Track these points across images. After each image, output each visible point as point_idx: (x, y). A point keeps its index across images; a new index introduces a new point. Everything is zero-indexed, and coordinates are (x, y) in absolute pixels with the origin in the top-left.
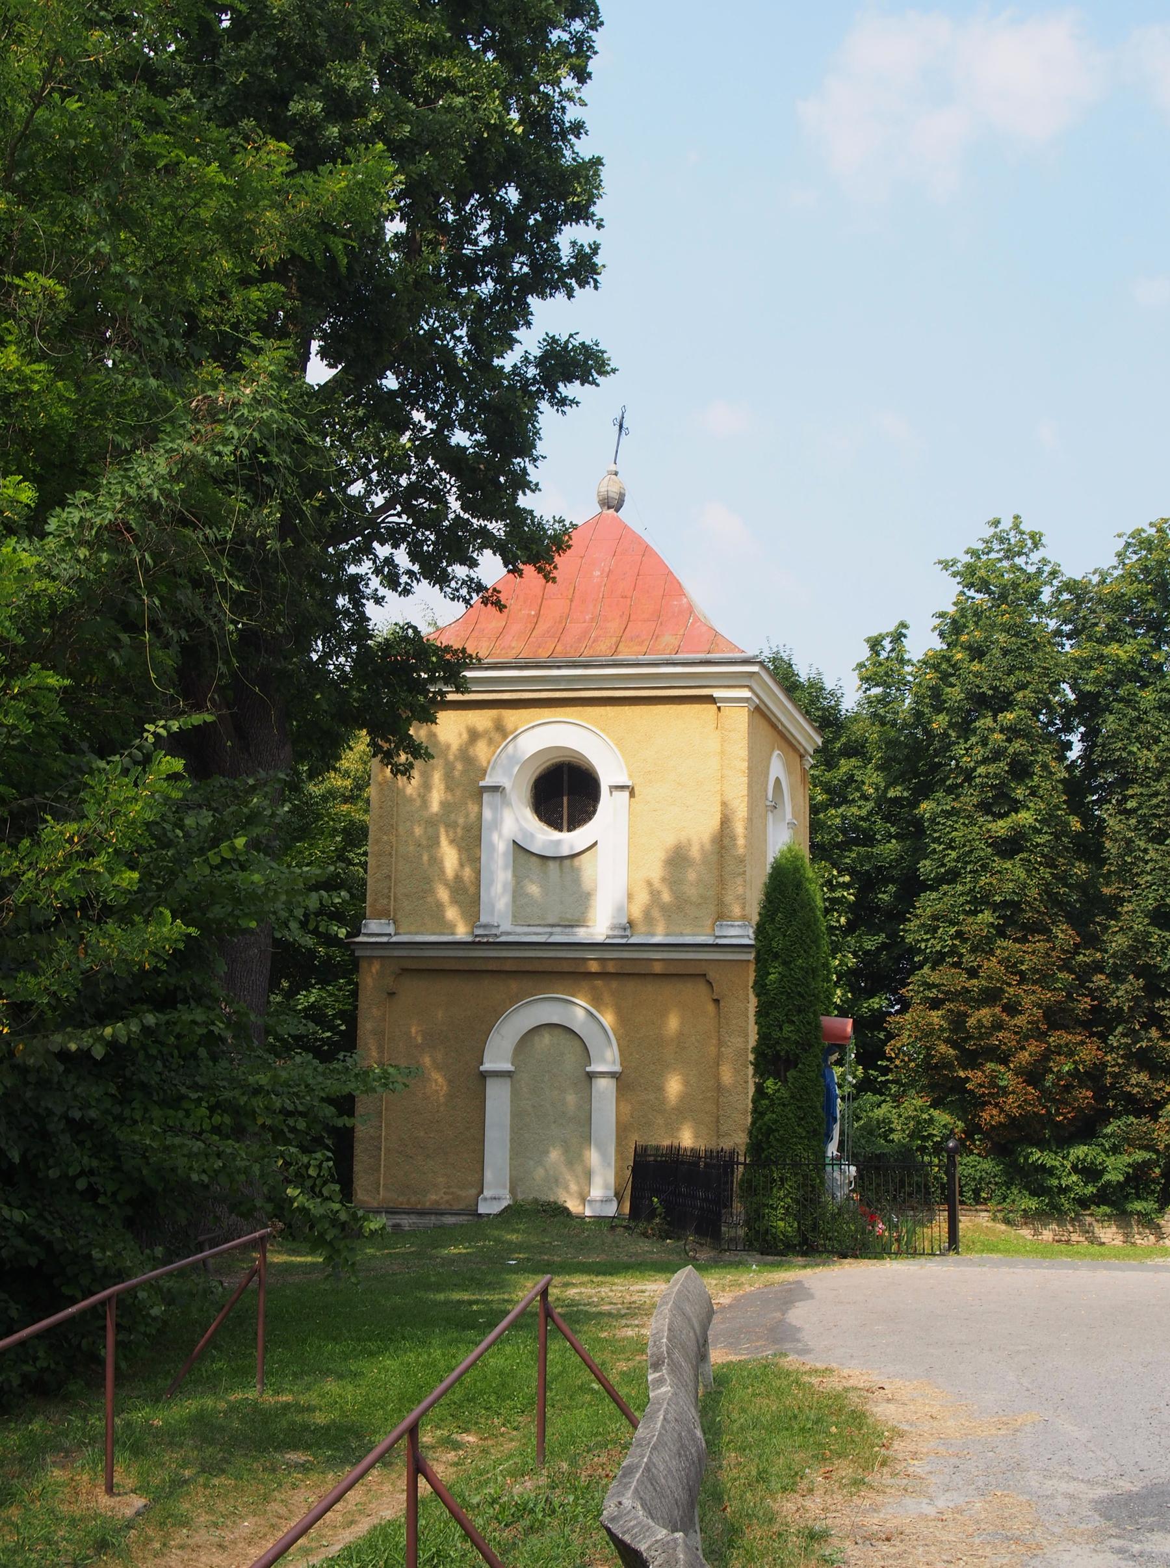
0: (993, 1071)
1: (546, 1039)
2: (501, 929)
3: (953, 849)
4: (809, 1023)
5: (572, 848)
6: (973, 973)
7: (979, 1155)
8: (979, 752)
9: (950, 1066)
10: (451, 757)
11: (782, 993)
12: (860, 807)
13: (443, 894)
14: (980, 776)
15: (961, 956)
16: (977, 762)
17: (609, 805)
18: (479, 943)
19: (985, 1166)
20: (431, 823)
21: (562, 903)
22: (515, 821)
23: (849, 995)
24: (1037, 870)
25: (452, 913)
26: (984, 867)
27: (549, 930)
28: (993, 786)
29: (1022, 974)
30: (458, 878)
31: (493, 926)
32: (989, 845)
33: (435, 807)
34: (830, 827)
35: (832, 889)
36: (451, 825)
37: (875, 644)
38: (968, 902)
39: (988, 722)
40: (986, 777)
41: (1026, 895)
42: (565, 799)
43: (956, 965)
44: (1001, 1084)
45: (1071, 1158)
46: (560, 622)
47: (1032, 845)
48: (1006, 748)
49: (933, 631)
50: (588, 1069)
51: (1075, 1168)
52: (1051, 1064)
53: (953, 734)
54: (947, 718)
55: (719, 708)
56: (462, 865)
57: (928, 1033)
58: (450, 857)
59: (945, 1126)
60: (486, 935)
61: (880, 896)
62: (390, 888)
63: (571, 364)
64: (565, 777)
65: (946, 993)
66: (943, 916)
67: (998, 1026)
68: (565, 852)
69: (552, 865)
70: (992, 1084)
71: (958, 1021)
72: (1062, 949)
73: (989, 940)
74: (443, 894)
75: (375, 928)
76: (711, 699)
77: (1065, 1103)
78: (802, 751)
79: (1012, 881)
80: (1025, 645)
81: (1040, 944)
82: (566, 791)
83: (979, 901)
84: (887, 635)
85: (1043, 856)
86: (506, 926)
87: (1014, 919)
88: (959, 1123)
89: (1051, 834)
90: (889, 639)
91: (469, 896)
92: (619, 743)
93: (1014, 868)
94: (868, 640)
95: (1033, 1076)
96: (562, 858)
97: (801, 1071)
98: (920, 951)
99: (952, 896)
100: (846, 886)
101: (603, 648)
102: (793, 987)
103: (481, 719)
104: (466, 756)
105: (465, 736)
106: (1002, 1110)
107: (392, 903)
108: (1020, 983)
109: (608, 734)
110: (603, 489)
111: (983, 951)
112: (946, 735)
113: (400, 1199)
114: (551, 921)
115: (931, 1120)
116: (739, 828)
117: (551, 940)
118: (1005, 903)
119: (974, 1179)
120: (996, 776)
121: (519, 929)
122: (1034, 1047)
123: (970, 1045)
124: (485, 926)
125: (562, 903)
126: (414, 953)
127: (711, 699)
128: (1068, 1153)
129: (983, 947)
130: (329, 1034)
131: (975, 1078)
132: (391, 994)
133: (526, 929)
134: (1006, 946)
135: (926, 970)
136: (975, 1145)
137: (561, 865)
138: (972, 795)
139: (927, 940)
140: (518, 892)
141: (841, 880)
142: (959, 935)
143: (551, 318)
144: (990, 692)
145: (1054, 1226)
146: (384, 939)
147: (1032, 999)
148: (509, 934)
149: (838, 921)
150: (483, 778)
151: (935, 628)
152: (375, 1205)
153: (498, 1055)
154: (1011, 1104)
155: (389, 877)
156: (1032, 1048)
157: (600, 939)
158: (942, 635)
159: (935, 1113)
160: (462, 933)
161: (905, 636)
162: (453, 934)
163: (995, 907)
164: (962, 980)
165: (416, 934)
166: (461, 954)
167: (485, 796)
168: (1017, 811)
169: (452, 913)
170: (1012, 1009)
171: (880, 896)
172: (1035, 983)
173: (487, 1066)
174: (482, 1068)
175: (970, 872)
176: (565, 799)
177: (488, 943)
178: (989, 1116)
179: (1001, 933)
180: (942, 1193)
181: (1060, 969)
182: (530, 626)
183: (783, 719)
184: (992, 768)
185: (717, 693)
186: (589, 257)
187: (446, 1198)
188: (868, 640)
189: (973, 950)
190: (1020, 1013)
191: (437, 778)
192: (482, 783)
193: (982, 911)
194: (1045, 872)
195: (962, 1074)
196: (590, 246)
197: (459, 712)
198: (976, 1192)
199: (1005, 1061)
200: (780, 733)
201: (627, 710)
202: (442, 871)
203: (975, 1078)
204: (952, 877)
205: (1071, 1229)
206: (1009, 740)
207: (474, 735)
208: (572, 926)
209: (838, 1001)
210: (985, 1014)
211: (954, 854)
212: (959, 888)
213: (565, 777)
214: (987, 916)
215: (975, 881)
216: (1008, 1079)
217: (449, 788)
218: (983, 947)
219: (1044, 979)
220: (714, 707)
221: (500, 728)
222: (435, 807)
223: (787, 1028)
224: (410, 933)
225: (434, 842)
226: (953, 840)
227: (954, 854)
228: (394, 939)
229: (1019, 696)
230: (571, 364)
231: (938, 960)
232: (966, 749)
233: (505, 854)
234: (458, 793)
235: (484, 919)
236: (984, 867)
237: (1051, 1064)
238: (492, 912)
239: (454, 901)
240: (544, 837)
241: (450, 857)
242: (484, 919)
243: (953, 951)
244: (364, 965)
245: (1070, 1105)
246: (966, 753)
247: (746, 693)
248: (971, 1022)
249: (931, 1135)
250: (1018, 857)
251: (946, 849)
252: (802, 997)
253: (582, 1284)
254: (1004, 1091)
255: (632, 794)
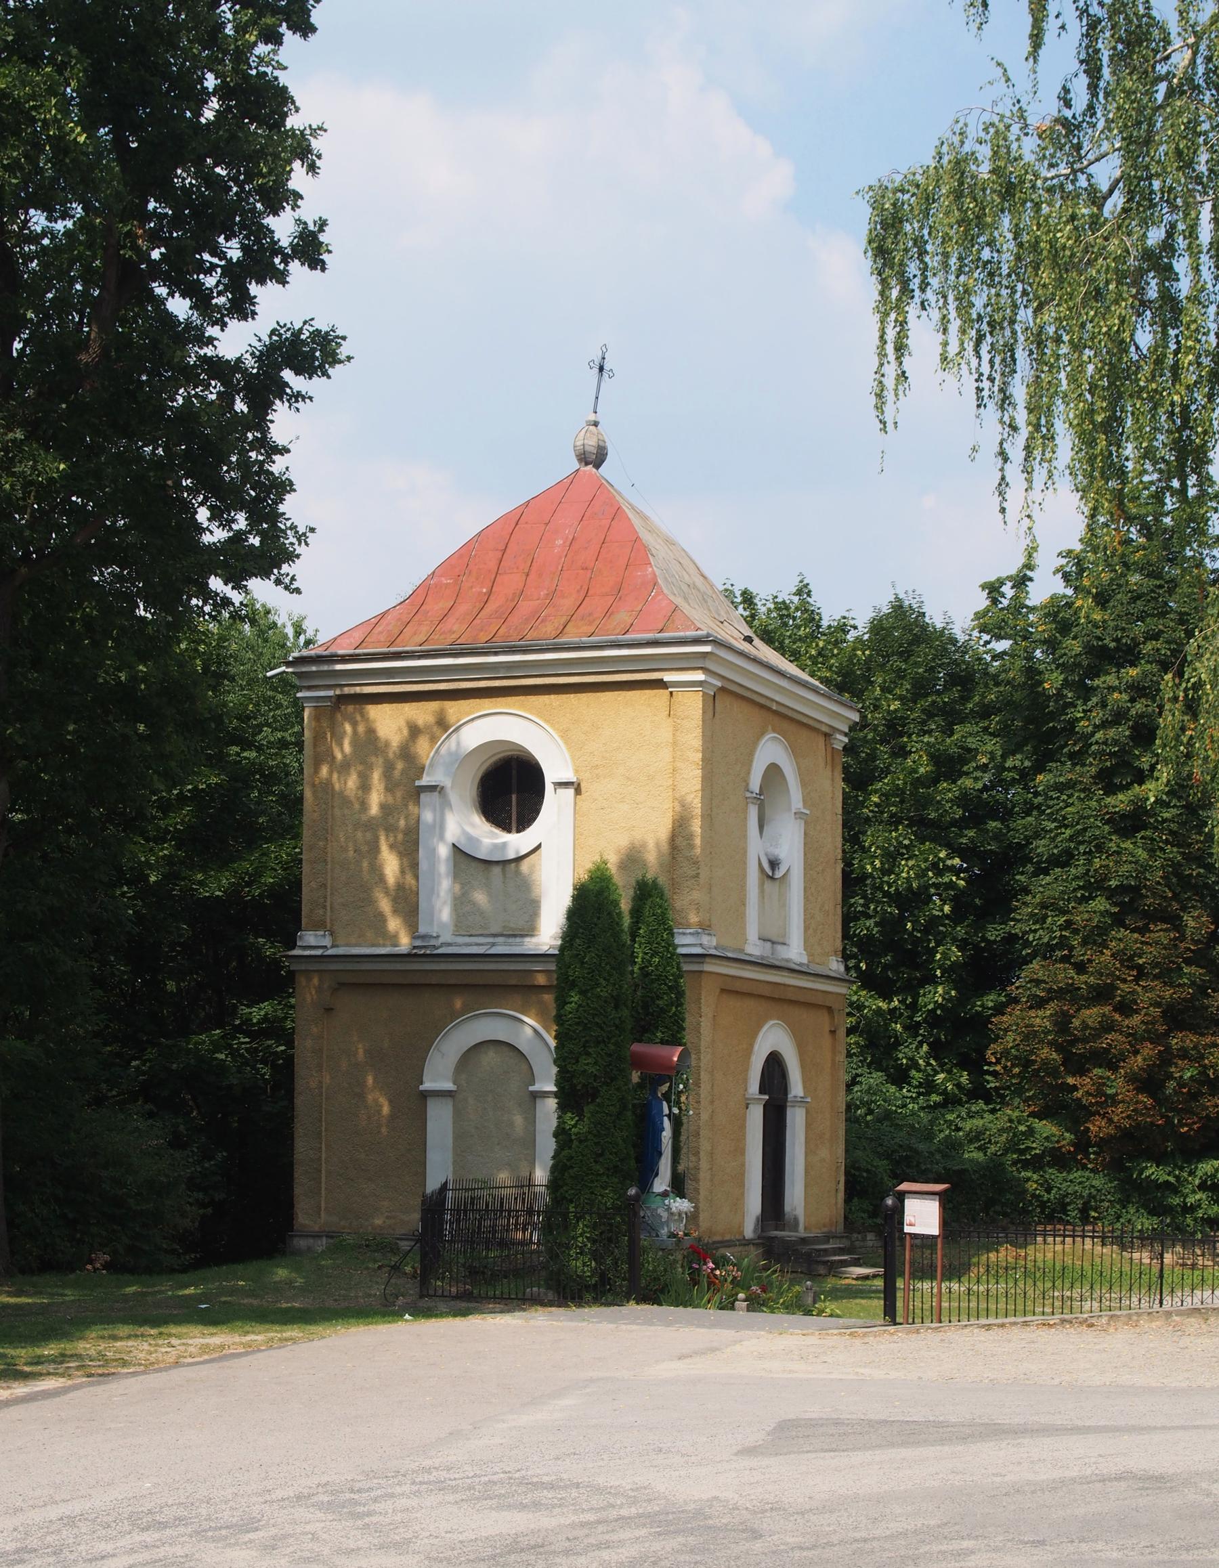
0: (1101, 1077)
1: (490, 1058)
2: (441, 940)
3: (1066, 827)
4: (610, 1055)
5: (517, 852)
6: (1081, 968)
7: (1092, 1171)
8: (1098, 716)
9: (1054, 1073)
10: (391, 755)
11: (577, 1024)
12: (976, 779)
13: (385, 905)
14: (1097, 743)
15: (1071, 949)
16: (1095, 726)
17: (554, 804)
18: (416, 955)
19: (1096, 1183)
20: (371, 826)
21: (505, 910)
22: (462, 824)
23: (953, 993)
24: (1162, 849)
25: (394, 924)
26: (1100, 848)
27: (491, 940)
28: (1112, 754)
29: (1140, 968)
30: (400, 887)
31: (431, 937)
32: (1107, 822)
33: (374, 810)
34: (938, 802)
35: (940, 873)
36: (390, 829)
37: (993, 589)
38: (1080, 888)
39: (1111, 680)
40: (1105, 743)
41: (1145, 879)
42: (514, 797)
43: (1065, 959)
44: (1109, 1092)
45: (1199, 1173)
46: (512, 600)
47: (1156, 821)
48: (1129, 709)
49: (1054, 573)
50: (531, 1088)
51: (1202, 1187)
52: (1173, 1069)
53: (1070, 695)
54: (1062, 677)
55: (671, 693)
56: (403, 872)
57: (1030, 1035)
58: (391, 865)
59: (1047, 1138)
60: (424, 947)
61: (1018, 877)
62: (325, 897)
63: (309, 352)
64: (514, 772)
65: (1050, 990)
66: (1052, 904)
67: (1107, 1027)
68: (511, 855)
69: (497, 870)
70: (1100, 1093)
71: (1062, 1022)
72: (1192, 939)
73: (1102, 930)
74: (385, 905)
75: (311, 940)
76: (660, 684)
77: (1191, 1112)
78: (824, 729)
79: (1131, 862)
80: (1161, 587)
81: (1161, 933)
82: (511, 788)
83: (1094, 886)
84: (1010, 578)
85: (1171, 832)
86: (447, 937)
87: (1130, 904)
88: (1067, 1135)
89: (1183, 806)
90: (1009, 584)
91: (408, 903)
92: (565, 735)
93: (1135, 849)
94: (983, 587)
95: (1149, 1082)
96: (505, 863)
97: (599, 1105)
98: (1027, 944)
99: (1048, 886)
100: (957, 871)
101: (548, 630)
102: (590, 1018)
103: (422, 713)
104: (406, 753)
105: (406, 732)
106: (1110, 1121)
107: (329, 913)
108: (1137, 980)
109: (552, 725)
110: (579, 443)
111: (1095, 943)
112: (1059, 695)
113: (342, 1223)
114: (493, 931)
115: (1031, 1131)
116: (696, 827)
117: (493, 951)
118: (1122, 889)
119: (1082, 1197)
120: (1116, 742)
121: (460, 940)
122: (1148, 1050)
123: (1079, 1049)
124: (423, 937)
125: (505, 910)
126: (349, 967)
127: (660, 684)
128: (1196, 1168)
129: (1096, 937)
130: (283, 1048)
131: (1082, 1086)
132: (329, 1010)
133: (468, 940)
134: (1123, 938)
135: (1035, 965)
136: (1089, 1159)
137: (504, 871)
138: (1091, 764)
139: (1035, 931)
140: (461, 903)
141: (949, 862)
142: (1068, 924)
143: (280, 305)
144: (1113, 645)
145: (1178, 1249)
146: (319, 952)
147: (1150, 995)
148: (449, 945)
149: (942, 910)
150: (420, 777)
151: (1057, 571)
152: (317, 1228)
153: (438, 1075)
154: (1119, 1114)
155: (324, 886)
156: (1145, 1052)
157: (544, 949)
158: (1066, 577)
159: (1038, 1125)
160: (405, 943)
161: (1031, 579)
162: (396, 946)
163: (1111, 894)
164: (1065, 975)
165: (356, 945)
166: (399, 967)
167: (422, 796)
168: (1140, 784)
169: (394, 924)
170: (1126, 1008)
171: (1018, 877)
172: (1156, 977)
173: (427, 1085)
174: (422, 1088)
175: (1085, 853)
176: (514, 797)
177: (424, 955)
178: (1097, 1127)
179: (1118, 921)
180: (1042, 1212)
181: (1188, 962)
182: (479, 606)
183: (777, 698)
184: (1111, 733)
185: (668, 677)
186: (314, 235)
187: (388, 1222)
188: (983, 587)
189: (1084, 943)
190: (1137, 1012)
191: (376, 776)
192: (417, 783)
193: (1093, 899)
194: (1173, 852)
195: (1071, 1081)
196: (315, 223)
197: (394, 705)
198: (1084, 1211)
199: (1113, 1067)
200: (776, 713)
201: (585, 697)
202: (382, 879)
203: (1082, 1086)
204: (1064, 859)
205: (1199, 1252)
206: (1133, 700)
207: (415, 731)
208: (522, 936)
209: (940, 1000)
210: (1092, 1015)
211: (1068, 832)
212: (1073, 871)
213: (514, 772)
214: (1100, 904)
215: (1090, 862)
216: (1118, 1085)
217: (389, 789)
218: (1096, 937)
219: (1167, 974)
220: (666, 692)
221: (442, 723)
222: (374, 810)
223: (584, 1060)
224: (347, 945)
225: (375, 850)
226: (1065, 818)
227: (1068, 832)
228: (330, 952)
229: (1148, 648)
230: (309, 352)
231: (1045, 952)
232: (1084, 711)
233: (447, 860)
234: (399, 794)
235: (422, 930)
236: (1100, 848)
237: (1173, 1069)
238: (431, 922)
239: (395, 911)
240: (489, 838)
241: (391, 865)
242: (422, 930)
243: (1063, 943)
244: (301, 980)
245: (1197, 1115)
246: (1086, 718)
247: (699, 676)
248: (1076, 1022)
249: (1029, 1149)
250: (1139, 835)
251: (1060, 827)
252: (602, 1028)
253: (129, 1337)
254: (1113, 1100)
255: (578, 791)
